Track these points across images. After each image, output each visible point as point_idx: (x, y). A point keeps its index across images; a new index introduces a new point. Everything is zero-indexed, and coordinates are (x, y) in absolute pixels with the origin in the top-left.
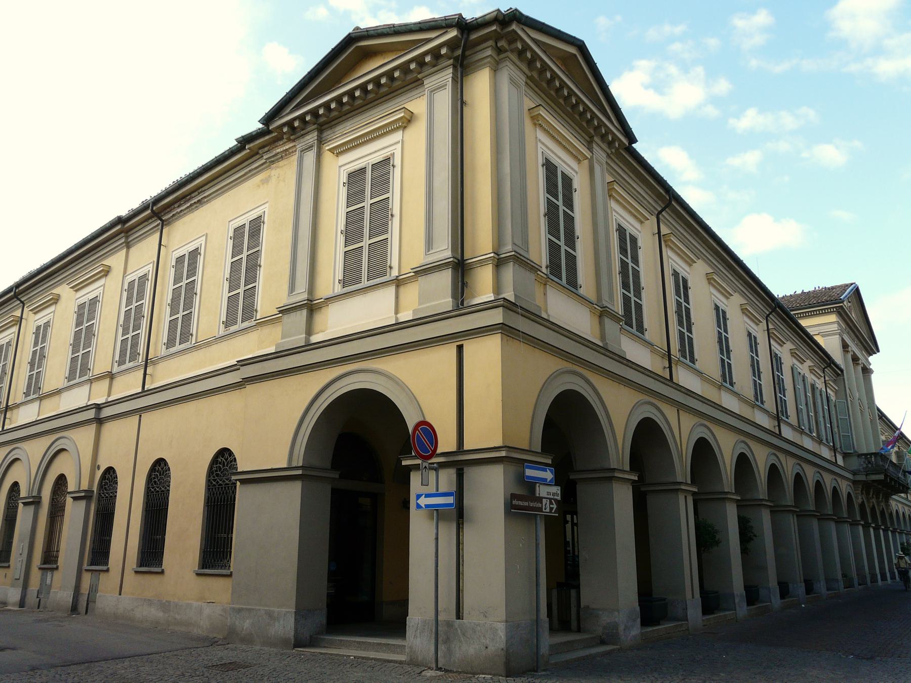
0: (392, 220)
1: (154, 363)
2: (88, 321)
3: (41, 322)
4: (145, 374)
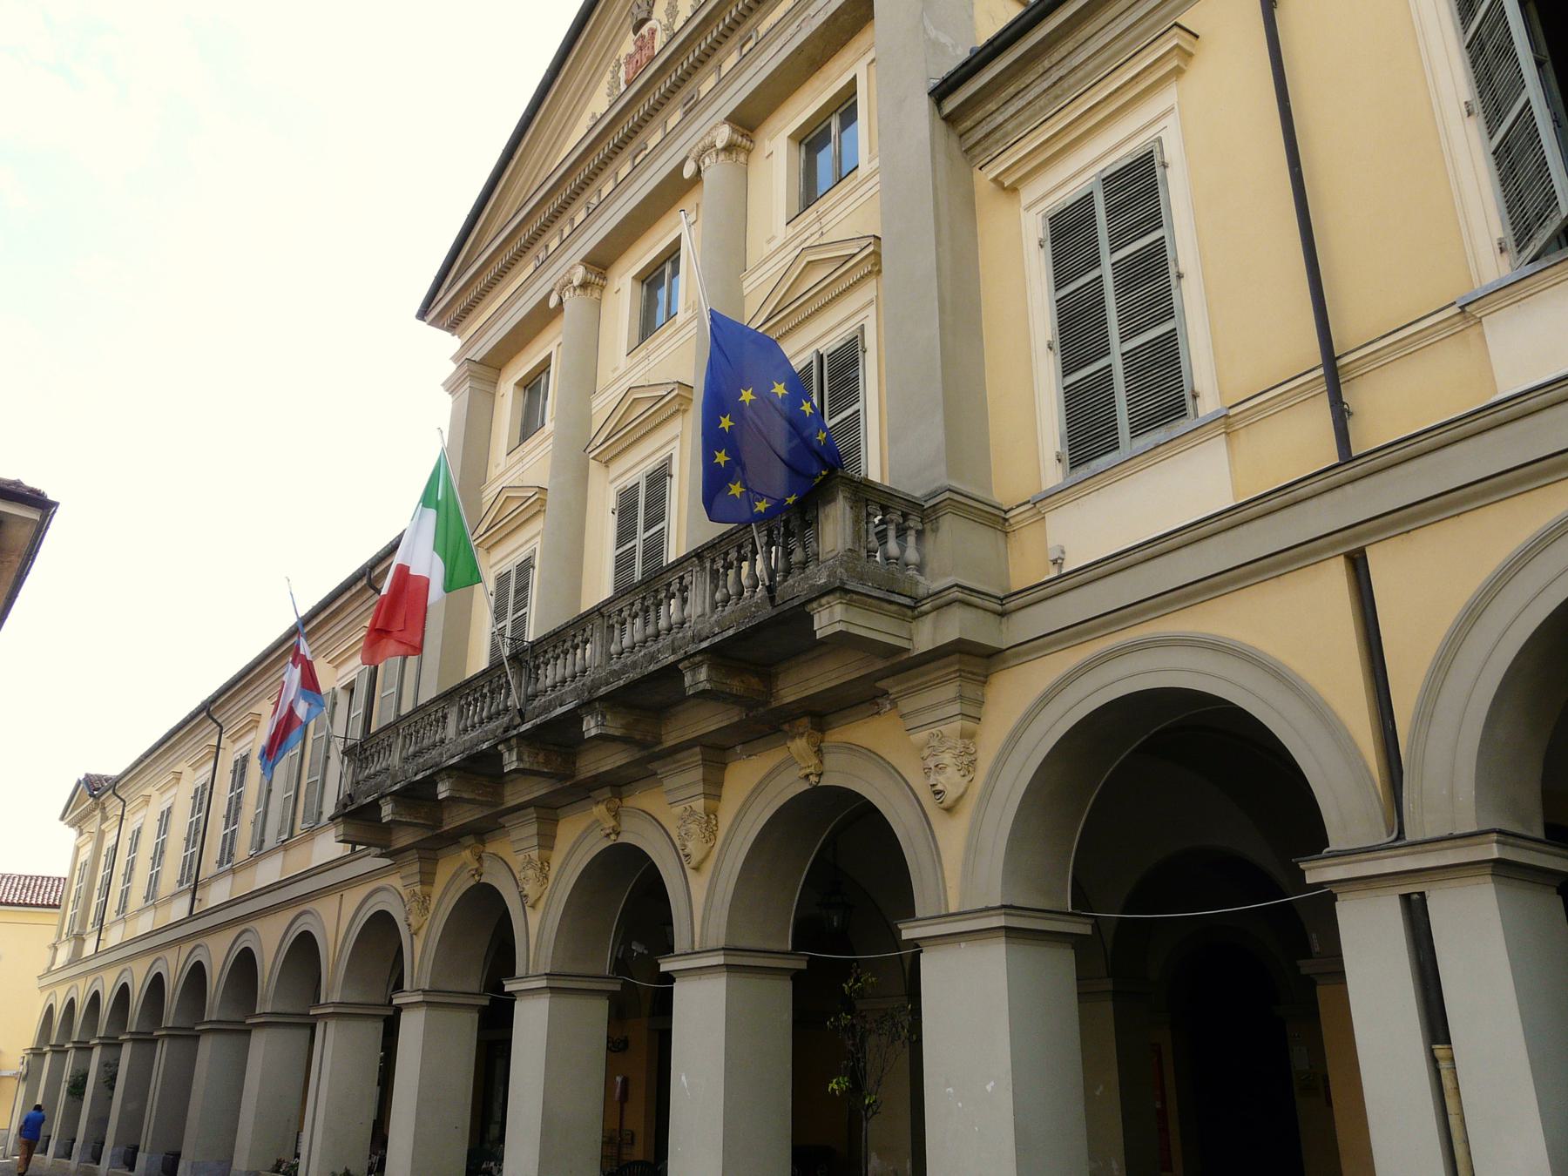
0: (1179, 286)
1: (204, 886)
2: (516, 611)
3: (510, 564)
4: (99, 940)
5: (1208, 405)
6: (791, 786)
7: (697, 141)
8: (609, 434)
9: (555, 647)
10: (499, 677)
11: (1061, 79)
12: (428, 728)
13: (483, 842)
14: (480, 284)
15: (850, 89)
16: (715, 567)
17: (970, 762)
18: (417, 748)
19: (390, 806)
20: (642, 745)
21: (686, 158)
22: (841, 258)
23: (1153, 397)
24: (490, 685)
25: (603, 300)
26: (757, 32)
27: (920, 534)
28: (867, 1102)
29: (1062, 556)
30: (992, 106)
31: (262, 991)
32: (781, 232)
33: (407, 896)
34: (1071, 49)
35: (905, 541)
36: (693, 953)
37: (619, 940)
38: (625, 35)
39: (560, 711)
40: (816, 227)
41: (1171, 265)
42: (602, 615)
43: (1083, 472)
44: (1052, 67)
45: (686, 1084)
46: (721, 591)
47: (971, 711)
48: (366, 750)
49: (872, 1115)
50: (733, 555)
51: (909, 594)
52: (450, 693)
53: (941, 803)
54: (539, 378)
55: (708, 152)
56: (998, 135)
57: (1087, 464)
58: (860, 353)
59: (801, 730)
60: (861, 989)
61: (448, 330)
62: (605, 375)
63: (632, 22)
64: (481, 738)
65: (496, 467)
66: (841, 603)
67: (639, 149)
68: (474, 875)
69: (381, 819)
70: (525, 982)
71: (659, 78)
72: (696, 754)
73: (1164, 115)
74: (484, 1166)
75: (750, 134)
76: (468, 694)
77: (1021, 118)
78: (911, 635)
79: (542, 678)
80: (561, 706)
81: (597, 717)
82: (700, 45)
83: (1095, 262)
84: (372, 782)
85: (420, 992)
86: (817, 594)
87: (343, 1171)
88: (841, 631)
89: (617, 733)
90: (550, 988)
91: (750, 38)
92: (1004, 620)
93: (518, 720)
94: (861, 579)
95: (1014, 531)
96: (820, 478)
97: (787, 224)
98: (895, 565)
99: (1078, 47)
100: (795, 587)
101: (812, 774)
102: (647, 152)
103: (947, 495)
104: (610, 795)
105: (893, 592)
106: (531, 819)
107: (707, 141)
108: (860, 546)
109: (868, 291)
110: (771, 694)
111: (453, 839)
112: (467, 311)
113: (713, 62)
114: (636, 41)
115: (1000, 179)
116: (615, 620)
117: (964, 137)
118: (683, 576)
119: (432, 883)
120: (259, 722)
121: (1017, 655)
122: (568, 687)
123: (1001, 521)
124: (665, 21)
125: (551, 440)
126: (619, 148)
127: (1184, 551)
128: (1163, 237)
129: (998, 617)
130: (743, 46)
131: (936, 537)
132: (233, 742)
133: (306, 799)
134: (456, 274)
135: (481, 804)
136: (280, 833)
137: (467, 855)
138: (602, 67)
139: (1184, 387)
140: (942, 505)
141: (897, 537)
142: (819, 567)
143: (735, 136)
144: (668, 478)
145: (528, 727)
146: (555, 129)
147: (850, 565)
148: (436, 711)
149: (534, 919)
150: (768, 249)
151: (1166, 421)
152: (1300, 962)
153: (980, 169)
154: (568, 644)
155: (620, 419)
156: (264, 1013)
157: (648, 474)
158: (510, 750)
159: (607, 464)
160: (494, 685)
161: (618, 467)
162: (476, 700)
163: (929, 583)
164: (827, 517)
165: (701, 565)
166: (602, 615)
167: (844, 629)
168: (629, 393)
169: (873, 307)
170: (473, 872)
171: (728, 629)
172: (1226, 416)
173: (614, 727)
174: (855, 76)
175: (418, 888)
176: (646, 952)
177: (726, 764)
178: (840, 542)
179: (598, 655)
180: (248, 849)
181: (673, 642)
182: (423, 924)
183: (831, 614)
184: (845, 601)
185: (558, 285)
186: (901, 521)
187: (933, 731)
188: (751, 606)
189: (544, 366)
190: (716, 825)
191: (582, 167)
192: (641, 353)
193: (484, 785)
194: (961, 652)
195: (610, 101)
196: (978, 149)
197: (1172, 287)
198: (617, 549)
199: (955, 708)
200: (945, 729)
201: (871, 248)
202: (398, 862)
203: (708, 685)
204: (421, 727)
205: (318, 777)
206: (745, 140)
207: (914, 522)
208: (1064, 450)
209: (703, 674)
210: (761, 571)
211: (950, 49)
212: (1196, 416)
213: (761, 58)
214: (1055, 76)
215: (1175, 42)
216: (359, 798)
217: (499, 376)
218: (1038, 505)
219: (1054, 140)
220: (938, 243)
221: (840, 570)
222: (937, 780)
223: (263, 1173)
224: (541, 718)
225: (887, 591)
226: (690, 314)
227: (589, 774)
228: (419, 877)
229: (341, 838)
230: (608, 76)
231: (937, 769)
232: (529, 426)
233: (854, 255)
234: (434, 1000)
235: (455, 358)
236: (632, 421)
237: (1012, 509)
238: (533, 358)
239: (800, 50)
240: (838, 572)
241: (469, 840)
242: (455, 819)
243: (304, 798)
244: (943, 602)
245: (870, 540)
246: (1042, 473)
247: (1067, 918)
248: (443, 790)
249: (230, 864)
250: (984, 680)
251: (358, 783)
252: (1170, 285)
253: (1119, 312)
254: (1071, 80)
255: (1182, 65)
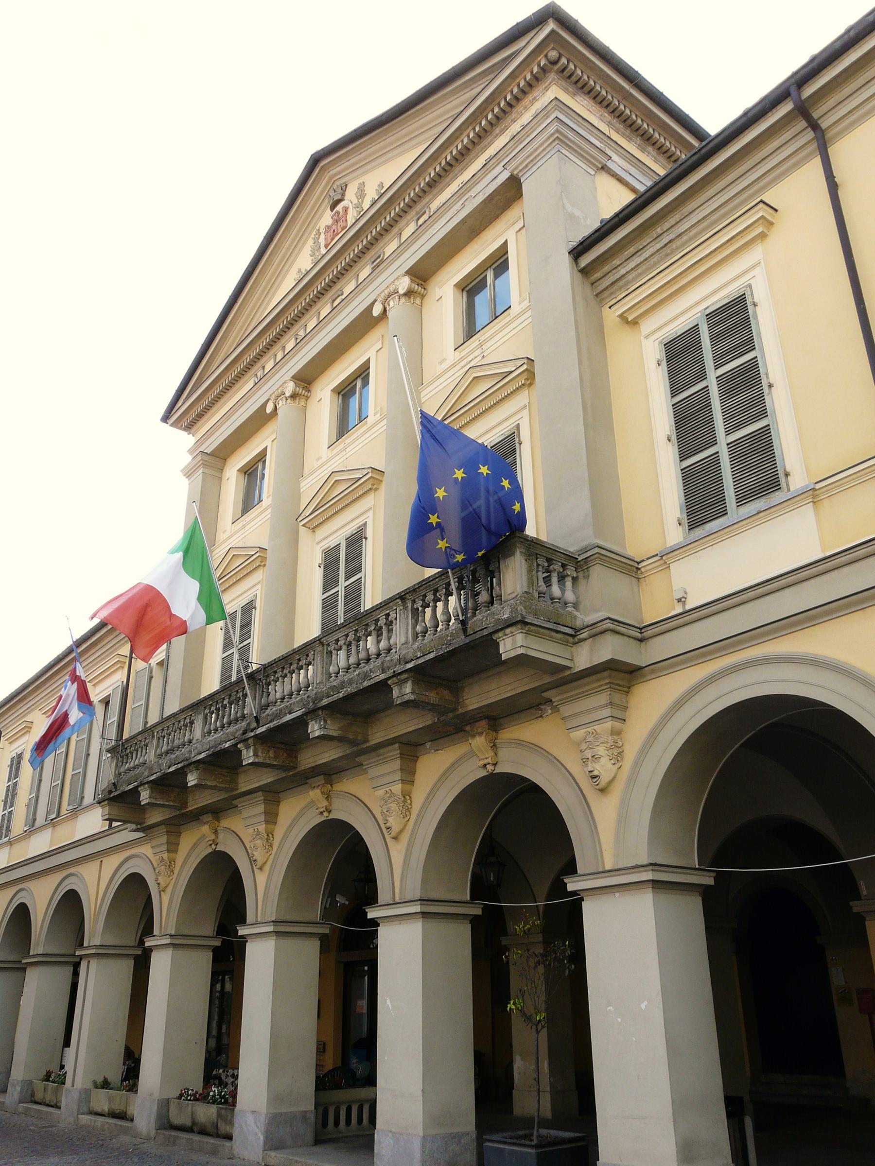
0: (770, 393)
5: (797, 481)
6: (471, 773)
7: (384, 288)
8: (315, 508)
9: (283, 668)
10: (237, 692)
11: (670, 241)
12: (178, 731)
13: (218, 819)
14: (211, 396)
15: (503, 250)
16: (415, 607)
17: (619, 753)
18: (169, 747)
19: (148, 792)
20: (353, 743)
21: (375, 301)
22: (501, 375)
23: (753, 476)
24: (229, 699)
25: (307, 408)
26: (430, 209)
27: (575, 580)
28: (538, 1019)
29: (685, 596)
30: (617, 262)
31: (35, 938)
32: (451, 356)
33: (156, 861)
34: (678, 220)
35: (564, 585)
36: (393, 904)
37: (327, 895)
38: (324, 211)
39: (289, 717)
40: (478, 352)
41: (763, 377)
42: (322, 644)
43: (699, 532)
44: (664, 232)
45: (390, 1006)
46: (420, 625)
47: (618, 714)
48: (126, 748)
49: (542, 1029)
50: (430, 597)
51: (570, 625)
52: (197, 704)
53: (597, 785)
54: (256, 466)
55: (393, 296)
56: (621, 283)
57: (701, 526)
58: (517, 445)
59: (480, 730)
60: (529, 929)
61: (184, 430)
62: (310, 463)
63: (329, 202)
64: (223, 739)
65: (224, 533)
66: (522, 632)
67: (336, 296)
68: (211, 845)
69: (140, 802)
70: (254, 927)
71: (354, 243)
72: (395, 751)
73: (753, 267)
74: (214, 1072)
75: (423, 283)
76: (211, 705)
77: (639, 271)
78: (572, 656)
79: (273, 693)
80: (290, 713)
81: (320, 722)
82: (385, 218)
83: (702, 375)
84: (132, 773)
85: (168, 936)
86: (502, 626)
87: (102, 1079)
88: (522, 654)
89: (335, 734)
90: (276, 932)
91: (425, 212)
92: (643, 644)
93: (254, 725)
94: (536, 615)
95: (645, 577)
96: (504, 538)
97: (455, 350)
98: (558, 604)
99: (683, 218)
100: (483, 620)
101: (489, 764)
102: (343, 297)
103: (597, 550)
104: (323, 782)
105: (559, 624)
106: (259, 801)
107: (392, 288)
108: (533, 589)
109: (522, 398)
110: (459, 703)
111: (196, 816)
112: (200, 416)
113: (395, 231)
114: (333, 216)
115: (625, 315)
116: (333, 647)
117: (595, 285)
118: (389, 613)
119: (176, 851)
120: (31, 728)
121: (653, 671)
122: (295, 699)
123: (635, 570)
124: (355, 201)
125: (269, 511)
126: (321, 294)
127: (787, 591)
128: (756, 357)
129: (639, 642)
130: (418, 219)
131: (587, 582)
132: (10, 743)
133: (71, 787)
134: (192, 388)
135: (221, 790)
136: (48, 813)
137: (205, 829)
138: (306, 234)
139: (778, 468)
140: (592, 558)
141: (558, 581)
142: (502, 606)
143: (413, 285)
144: (364, 540)
145: (263, 730)
146: (269, 281)
147: (527, 603)
148: (185, 718)
149: (262, 879)
150: (440, 369)
151: (764, 493)
152: (851, 903)
153: (610, 307)
154: (294, 666)
155: (323, 498)
156: (37, 954)
157: (348, 537)
158: (247, 747)
159: (313, 530)
160: (232, 699)
161: (321, 532)
162: (218, 710)
163: (584, 618)
164: (507, 567)
165: (404, 605)
166: (322, 644)
167: (524, 653)
168: (332, 476)
169: (526, 412)
170: (211, 843)
171: (430, 653)
172: (814, 489)
173: (333, 730)
174: (506, 241)
175: (165, 855)
176: (347, 903)
177: (418, 757)
178: (518, 586)
179: (319, 675)
180: (23, 825)
181: (382, 663)
182: (170, 883)
183: (514, 641)
184: (525, 631)
185: (273, 396)
186: (562, 570)
187: (589, 730)
188: (447, 636)
189: (261, 457)
190: (411, 804)
191: (292, 309)
192: (340, 445)
193: (224, 776)
194: (611, 669)
195: (312, 260)
196: (606, 293)
197: (765, 394)
198: (323, 594)
199: (607, 712)
200: (598, 728)
201: (525, 367)
202: (149, 835)
203: (412, 696)
204: (172, 731)
205: (81, 770)
206: (420, 288)
207: (570, 571)
208: (683, 516)
209: (408, 688)
210: (455, 608)
211: (582, 220)
212: (789, 490)
213: (433, 228)
214: (666, 240)
215: (761, 215)
216: (122, 785)
217: (225, 465)
218: (664, 558)
219: (667, 286)
220: (580, 362)
221: (520, 608)
222: (593, 767)
223: (35, 1081)
224: (274, 723)
225: (554, 623)
226: (378, 417)
227: (308, 766)
228: (166, 846)
229: (107, 817)
230: (310, 242)
231: (594, 759)
232: (248, 503)
233: (512, 372)
234: (179, 942)
235: (191, 451)
236: (327, 503)
237: (643, 561)
238: (243, 458)
239: (463, 221)
240: (519, 609)
241: (208, 817)
242: (195, 803)
243: (69, 786)
244: (597, 631)
245: (539, 585)
246: (666, 534)
247: (695, 872)
248: (192, 779)
249: (8, 838)
250: (627, 690)
251: (120, 774)
252: (763, 393)
253: (723, 413)
254: (678, 242)
255: (766, 231)
